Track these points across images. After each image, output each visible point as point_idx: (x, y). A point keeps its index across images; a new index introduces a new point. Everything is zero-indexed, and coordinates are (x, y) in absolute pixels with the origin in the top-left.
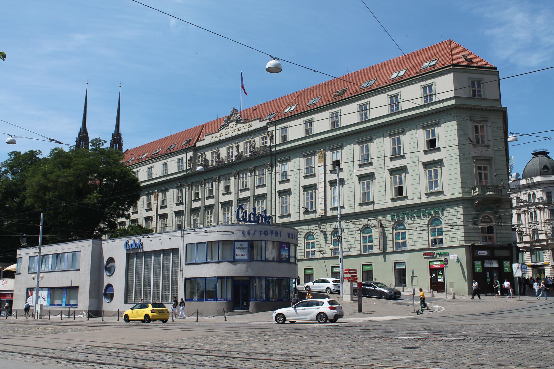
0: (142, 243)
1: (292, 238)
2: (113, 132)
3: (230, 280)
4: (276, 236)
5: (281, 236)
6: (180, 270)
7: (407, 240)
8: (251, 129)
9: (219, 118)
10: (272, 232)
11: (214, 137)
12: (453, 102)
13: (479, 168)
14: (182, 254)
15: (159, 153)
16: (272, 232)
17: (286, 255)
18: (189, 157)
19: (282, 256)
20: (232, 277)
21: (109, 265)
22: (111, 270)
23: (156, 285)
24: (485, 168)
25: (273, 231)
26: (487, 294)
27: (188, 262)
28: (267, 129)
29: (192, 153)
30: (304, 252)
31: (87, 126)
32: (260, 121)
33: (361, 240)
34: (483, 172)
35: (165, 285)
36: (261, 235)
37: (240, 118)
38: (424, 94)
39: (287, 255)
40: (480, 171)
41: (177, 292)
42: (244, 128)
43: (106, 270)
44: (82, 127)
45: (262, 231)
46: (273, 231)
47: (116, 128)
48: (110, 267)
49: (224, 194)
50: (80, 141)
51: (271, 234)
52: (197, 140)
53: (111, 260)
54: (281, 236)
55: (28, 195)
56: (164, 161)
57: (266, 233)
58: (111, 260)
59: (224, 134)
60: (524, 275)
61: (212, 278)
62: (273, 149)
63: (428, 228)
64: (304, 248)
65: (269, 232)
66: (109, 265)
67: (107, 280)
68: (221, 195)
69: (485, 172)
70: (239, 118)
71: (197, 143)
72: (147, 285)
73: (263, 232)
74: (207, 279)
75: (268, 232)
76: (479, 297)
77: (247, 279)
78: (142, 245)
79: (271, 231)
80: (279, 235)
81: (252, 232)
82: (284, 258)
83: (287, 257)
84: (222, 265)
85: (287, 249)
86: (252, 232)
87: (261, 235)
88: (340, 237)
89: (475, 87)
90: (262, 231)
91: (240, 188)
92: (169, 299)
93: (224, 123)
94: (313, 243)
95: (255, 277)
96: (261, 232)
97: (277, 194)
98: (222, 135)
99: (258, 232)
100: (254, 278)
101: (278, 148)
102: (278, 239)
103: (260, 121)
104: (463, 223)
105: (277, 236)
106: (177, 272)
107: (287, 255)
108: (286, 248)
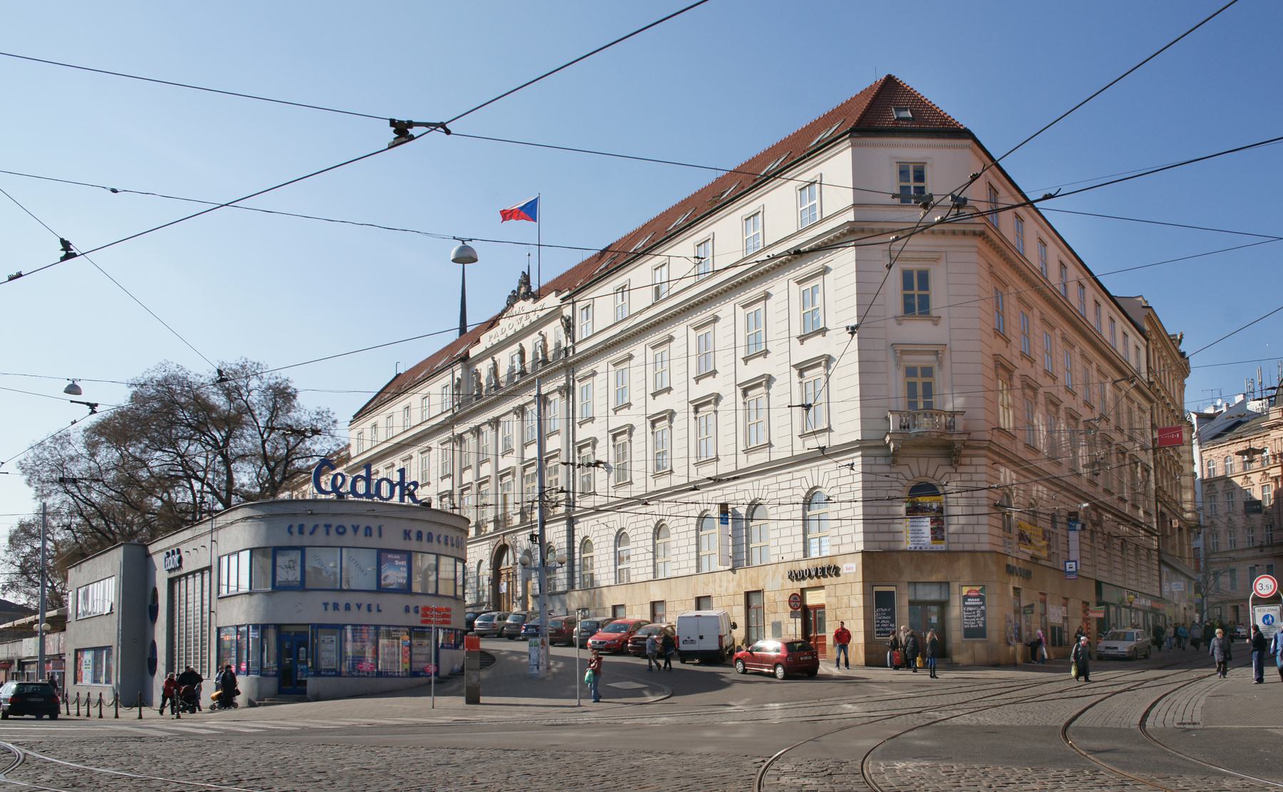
4: (366, 535)
5: (380, 535)
10: (356, 529)
12: (850, 216)
13: (910, 372)
24: (928, 372)
25: (358, 526)
26: (491, 587)
34: (920, 381)
36: (328, 533)
39: (403, 578)
40: (912, 380)
45: (330, 526)
46: (358, 526)
51: (353, 533)
54: (380, 535)
55: (740, 644)
57: (341, 530)
59: (507, 329)
60: (406, 556)
62: (60, 698)
69: (928, 380)
73: (333, 531)
75: (340, 527)
76: (933, 676)
79: (353, 526)
87: (328, 533)
89: (912, 289)
90: (330, 526)
94: (592, 557)
96: (328, 527)
101: (578, 350)
102: (375, 541)
105: (371, 535)
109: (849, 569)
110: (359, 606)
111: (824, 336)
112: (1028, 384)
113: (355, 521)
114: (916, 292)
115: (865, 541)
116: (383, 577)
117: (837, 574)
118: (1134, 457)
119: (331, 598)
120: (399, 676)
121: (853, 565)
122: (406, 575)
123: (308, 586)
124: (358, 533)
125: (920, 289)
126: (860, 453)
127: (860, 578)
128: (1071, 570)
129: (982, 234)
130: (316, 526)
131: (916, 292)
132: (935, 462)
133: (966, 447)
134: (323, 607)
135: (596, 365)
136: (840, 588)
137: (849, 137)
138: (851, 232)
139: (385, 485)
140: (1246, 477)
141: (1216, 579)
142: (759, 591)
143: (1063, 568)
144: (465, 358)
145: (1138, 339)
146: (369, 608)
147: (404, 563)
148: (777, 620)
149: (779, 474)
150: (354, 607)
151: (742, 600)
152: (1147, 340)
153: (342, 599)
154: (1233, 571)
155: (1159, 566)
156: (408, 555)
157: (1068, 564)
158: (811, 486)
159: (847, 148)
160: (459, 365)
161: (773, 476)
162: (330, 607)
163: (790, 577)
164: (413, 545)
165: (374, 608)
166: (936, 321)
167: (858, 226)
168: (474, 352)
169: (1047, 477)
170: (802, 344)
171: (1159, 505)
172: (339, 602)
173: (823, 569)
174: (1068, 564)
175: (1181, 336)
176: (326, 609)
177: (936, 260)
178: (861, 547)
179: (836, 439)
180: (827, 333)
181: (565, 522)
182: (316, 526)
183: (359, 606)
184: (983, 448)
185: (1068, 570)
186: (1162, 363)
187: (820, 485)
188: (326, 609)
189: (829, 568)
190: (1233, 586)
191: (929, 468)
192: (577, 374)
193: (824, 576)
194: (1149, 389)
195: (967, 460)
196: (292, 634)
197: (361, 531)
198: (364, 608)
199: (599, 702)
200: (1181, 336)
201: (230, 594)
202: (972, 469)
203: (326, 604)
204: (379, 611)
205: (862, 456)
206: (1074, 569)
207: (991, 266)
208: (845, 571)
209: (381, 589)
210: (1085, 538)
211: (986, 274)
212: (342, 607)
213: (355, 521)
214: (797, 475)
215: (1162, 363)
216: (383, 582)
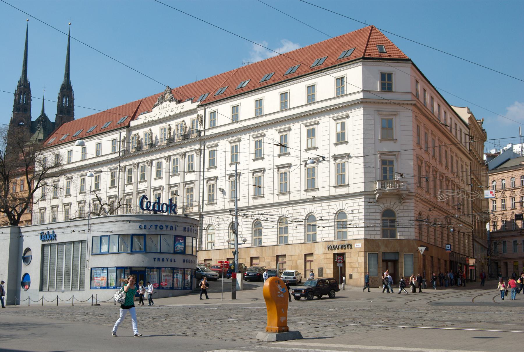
0: (56, 235)
1: (188, 231)
2: (62, 84)
3: (128, 270)
5: (176, 229)
6: (87, 261)
7: (263, 237)
8: (182, 111)
9: (156, 94)
10: (167, 227)
11: (148, 117)
14: (89, 244)
15: (93, 132)
16: (156, 226)
17: (181, 247)
18: (122, 138)
19: (176, 248)
20: (131, 268)
21: (27, 255)
22: (27, 260)
23: (67, 274)
27: (93, 253)
28: (197, 112)
29: (125, 133)
30: (252, 240)
31: (28, 76)
32: (192, 103)
33: (252, 234)
35: (74, 274)
37: (173, 98)
38: (145, 173)
39: (183, 248)
41: (84, 281)
42: (176, 109)
43: (24, 261)
44: (22, 77)
46: (168, 226)
47: (65, 78)
48: (28, 257)
49: (155, 179)
50: (20, 93)
52: (133, 119)
53: (28, 250)
54: (176, 229)
56: (98, 141)
57: (161, 227)
58: (28, 250)
59: (158, 114)
61: (112, 268)
63: (277, 226)
64: (252, 235)
65: (165, 227)
66: (27, 255)
67: (25, 269)
68: (153, 180)
70: (172, 98)
71: (131, 122)
72: (59, 274)
73: (158, 227)
74: (109, 268)
75: (163, 227)
77: (144, 269)
78: (55, 236)
79: (166, 226)
80: (174, 229)
81: (148, 227)
82: (179, 250)
83: (183, 249)
84: (121, 256)
85: (183, 241)
86: (148, 227)
88: (235, 230)
89: (385, 80)
91: (171, 174)
92: (77, 287)
93: (158, 102)
95: (160, 267)
96: (156, 226)
97: (205, 181)
98: (155, 115)
99: (154, 226)
100: (152, 268)
101: (207, 133)
103: (192, 103)
104: (363, 217)
105: (172, 230)
106: (85, 262)
107: (183, 248)
108: (181, 241)
109: (358, 246)
110: (167, 260)
111: (347, 145)
112: (419, 159)
113: (167, 224)
114: (386, 81)
115: (365, 234)
116: (176, 247)
117: (351, 248)
118: (459, 186)
119: (157, 256)
120: (178, 289)
121: (360, 244)
122: (183, 246)
123: (147, 250)
124: (168, 229)
125: (388, 81)
126: (363, 197)
127: (363, 250)
128: (448, 248)
129: (415, 105)
130: (152, 226)
131: (386, 81)
132: (393, 202)
133: (408, 195)
134: (154, 260)
135: (219, 141)
136: (353, 254)
137: (362, 61)
138: (362, 102)
139: (165, 206)
140: (512, 191)
141: (496, 247)
142: (313, 254)
143: (445, 248)
144: (128, 126)
145: (466, 129)
146: (159, 259)
147: (183, 241)
148: (321, 267)
149: (323, 203)
150: (165, 260)
151: (303, 257)
152: (469, 129)
153: (161, 256)
154: (505, 242)
155: (473, 242)
156: (184, 238)
157: (447, 246)
158: (339, 209)
159: (360, 65)
160: (125, 130)
161: (320, 203)
162: (156, 260)
163: (328, 248)
164: (186, 234)
165: (173, 261)
166: (395, 141)
167: (365, 100)
168: (133, 124)
169: (422, 198)
170: (336, 147)
171: (473, 212)
172: (160, 258)
173: (345, 245)
174: (447, 246)
175: (483, 120)
176: (155, 261)
177: (396, 115)
178: (363, 236)
179: (352, 190)
180: (348, 144)
181: (198, 216)
182: (152, 226)
183: (167, 260)
184: (413, 196)
185: (447, 248)
186: (478, 144)
187: (343, 209)
188: (155, 261)
189: (348, 245)
190: (504, 251)
191: (392, 204)
192: (207, 144)
193: (345, 248)
194: (470, 154)
195: (406, 201)
196: (138, 271)
197: (169, 228)
198: (169, 260)
199: (334, 297)
200: (483, 120)
201: (101, 253)
202: (408, 204)
203: (155, 259)
204: (175, 261)
205: (364, 198)
206: (449, 248)
207: (425, 124)
208: (356, 247)
209: (175, 252)
210: (445, 231)
211: (414, 120)
212: (161, 260)
213: (167, 224)
214: (332, 203)
215: (478, 144)
216: (176, 249)
